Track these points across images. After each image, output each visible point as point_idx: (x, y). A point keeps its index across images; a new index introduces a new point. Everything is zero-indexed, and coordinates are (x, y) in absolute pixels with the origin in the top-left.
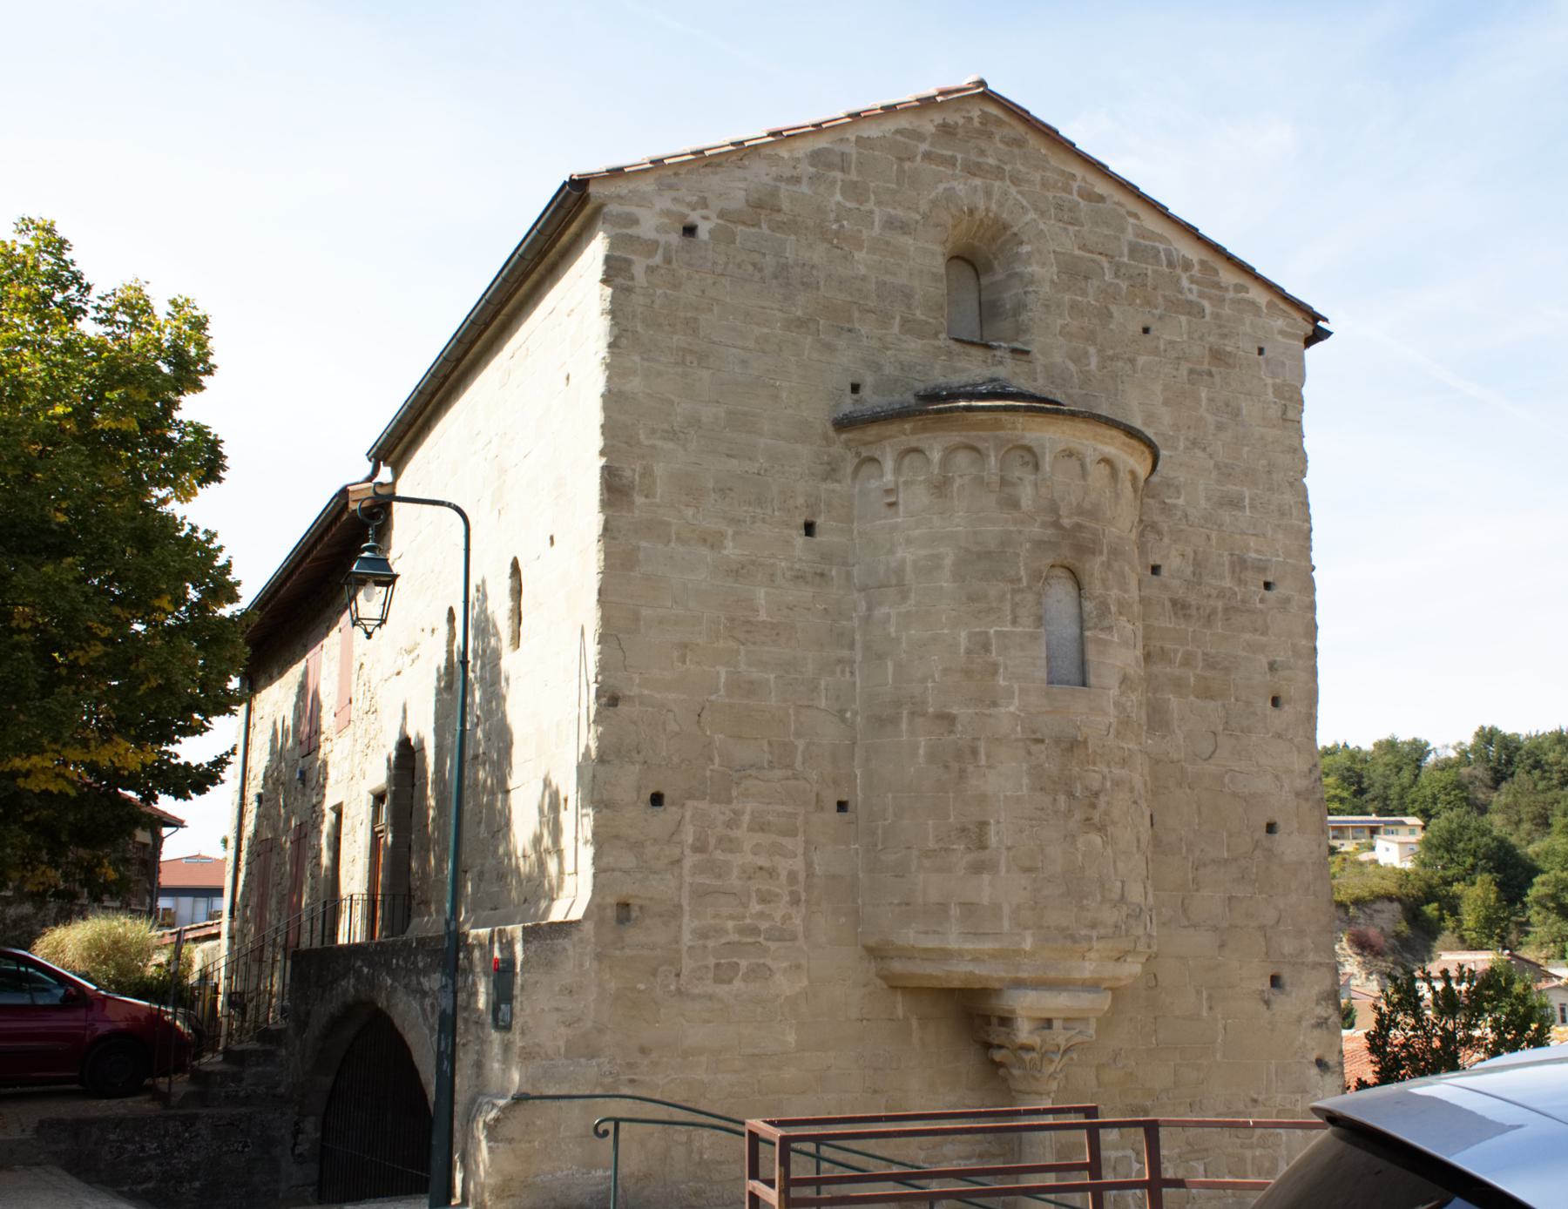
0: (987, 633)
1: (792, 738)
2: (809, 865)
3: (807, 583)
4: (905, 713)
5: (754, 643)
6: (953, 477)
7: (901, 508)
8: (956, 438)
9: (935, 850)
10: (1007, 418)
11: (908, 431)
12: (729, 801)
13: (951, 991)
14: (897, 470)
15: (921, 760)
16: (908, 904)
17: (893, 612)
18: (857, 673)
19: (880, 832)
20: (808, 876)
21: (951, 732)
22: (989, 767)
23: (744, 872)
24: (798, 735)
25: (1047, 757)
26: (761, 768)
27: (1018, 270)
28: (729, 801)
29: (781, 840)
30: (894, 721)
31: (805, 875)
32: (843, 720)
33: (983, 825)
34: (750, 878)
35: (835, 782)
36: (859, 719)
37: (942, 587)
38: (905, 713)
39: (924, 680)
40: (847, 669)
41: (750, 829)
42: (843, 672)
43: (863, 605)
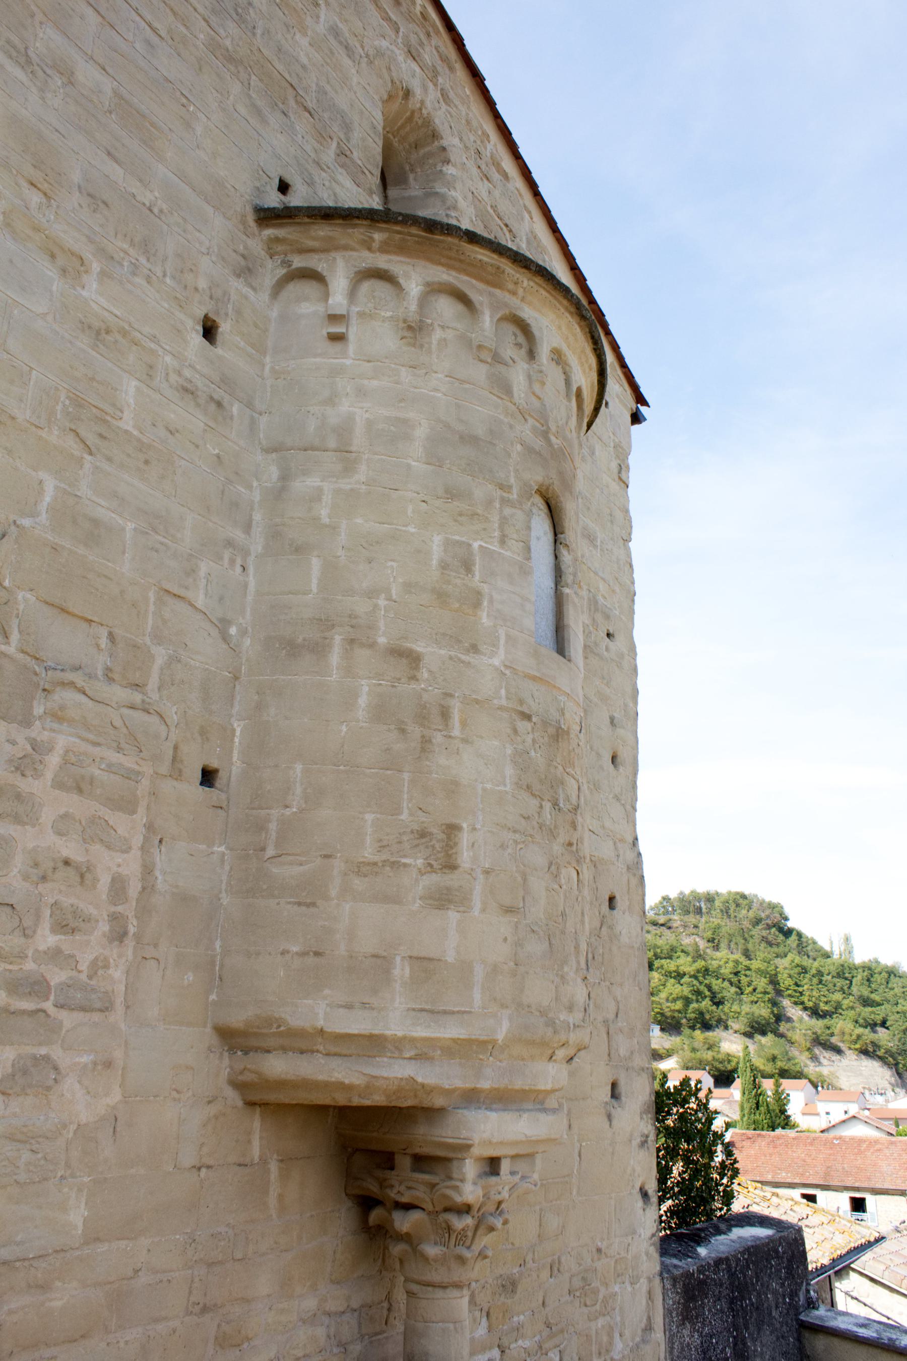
0: (470, 545)
1: (148, 640)
2: (148, 870)
3: (198, 405)
4: (338, 639)
5: (109, 459)
6: (432, 324)
7: (352, 348)
8: (444, 275)
9: (375, 864)
10: (512, 272)
11: (376, 245)
12: (26, 722)
13: (322, 1109)
14: (352, 293)
15: (361, 714)
16: (317, 954)
17: (327, 486)
18: (251, 570)
19: (273, 826)
20: (144, 889)
21: (413, 678)
22: (465, 741)
23: (36, 865)
24: (158, 638)
25: (534, 741)
26: (91, 676)
27: (438, 190)
28: (26, 722)
29: (105, 813)
30: (319, 649)
31: (139, 888)
32: (225, 637)
33: (452, 829)
34: (44, 878)
35: (203, 732)
36: (247, 642)
37: (409, 466)
38: (338, 639)
39: (371, 594)
40: (239, 561)
41: (58, 785)
42: (232, 562)
43: (274, 472)
